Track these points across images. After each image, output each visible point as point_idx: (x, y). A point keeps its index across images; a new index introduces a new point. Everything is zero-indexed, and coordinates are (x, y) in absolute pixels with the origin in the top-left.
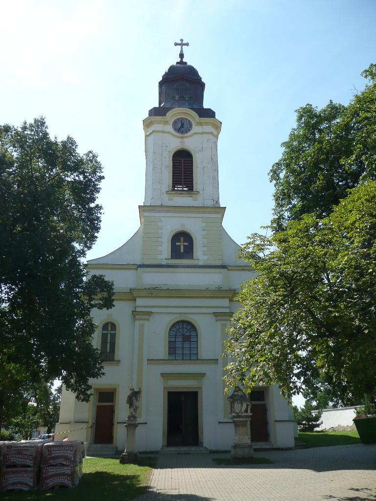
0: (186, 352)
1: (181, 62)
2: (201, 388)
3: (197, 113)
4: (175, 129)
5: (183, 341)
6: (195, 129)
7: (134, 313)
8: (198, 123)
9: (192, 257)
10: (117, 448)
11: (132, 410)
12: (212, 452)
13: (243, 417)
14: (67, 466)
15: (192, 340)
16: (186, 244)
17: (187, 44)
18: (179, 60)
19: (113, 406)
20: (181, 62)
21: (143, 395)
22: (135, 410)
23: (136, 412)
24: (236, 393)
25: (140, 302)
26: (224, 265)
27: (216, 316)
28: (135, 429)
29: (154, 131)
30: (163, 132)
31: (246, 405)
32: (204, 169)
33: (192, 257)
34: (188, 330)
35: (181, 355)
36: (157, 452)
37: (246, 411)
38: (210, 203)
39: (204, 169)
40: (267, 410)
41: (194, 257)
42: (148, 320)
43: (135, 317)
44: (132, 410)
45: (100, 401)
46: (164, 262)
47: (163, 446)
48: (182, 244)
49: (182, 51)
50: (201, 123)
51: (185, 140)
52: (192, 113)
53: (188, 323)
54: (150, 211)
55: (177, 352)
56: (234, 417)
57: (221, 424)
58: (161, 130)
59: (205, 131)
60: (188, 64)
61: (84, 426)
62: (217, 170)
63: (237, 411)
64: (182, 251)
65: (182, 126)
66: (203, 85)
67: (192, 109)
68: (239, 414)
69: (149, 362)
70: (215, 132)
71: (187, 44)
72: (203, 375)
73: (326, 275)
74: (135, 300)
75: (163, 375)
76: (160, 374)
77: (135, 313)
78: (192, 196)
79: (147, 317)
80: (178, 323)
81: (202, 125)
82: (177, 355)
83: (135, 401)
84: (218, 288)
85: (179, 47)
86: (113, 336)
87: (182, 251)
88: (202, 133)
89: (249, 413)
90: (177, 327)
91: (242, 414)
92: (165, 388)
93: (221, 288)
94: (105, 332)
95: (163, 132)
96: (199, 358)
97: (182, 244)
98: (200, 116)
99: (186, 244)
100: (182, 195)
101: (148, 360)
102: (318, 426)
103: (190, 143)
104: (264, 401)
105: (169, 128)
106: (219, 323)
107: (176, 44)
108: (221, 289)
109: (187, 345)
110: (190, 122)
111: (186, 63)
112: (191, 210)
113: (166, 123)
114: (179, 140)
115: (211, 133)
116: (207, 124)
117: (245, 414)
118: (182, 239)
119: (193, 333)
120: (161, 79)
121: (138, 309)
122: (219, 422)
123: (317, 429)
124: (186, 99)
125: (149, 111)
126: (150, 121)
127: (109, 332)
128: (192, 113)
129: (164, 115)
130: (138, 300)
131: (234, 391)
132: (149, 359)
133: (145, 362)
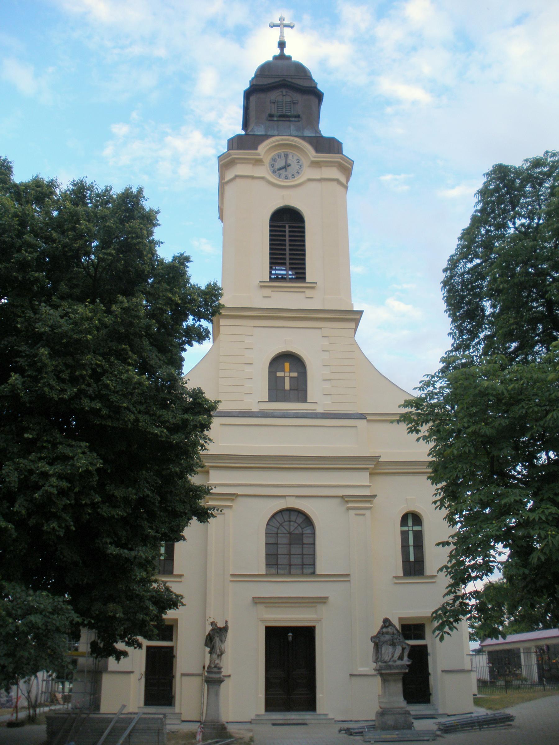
0: (296, 560)
1: (282, 57)
5: (290, 544)
9: (303, 398)
13: (397, 667)
14: (133, 413)
15: (305, 541)
16: (295, 374)
18: (277, 52)
20: (282, 57)
23: (221, 660)
24: (384, 630)
28: (220, 685)
31: (400, 648)
33: (303, 398)
34: (299, 525)
35: (299, 556)
37: (401, 658)
41: (309, 400)
46: (255, 408)
49: (282, 35)
53: (299, 512)
55: (280, 562)
57: (354, 679)
60: (293, 59)
63: (387, 658)
64: (287, 387)
66: (319, 96)
67: (303, 138)
70: (343, 179)
72: (323, 600)
75: (257, 601)
76: (251, 598)
80: (281, 512)
81: (320, 167)
82: (304, 546)
83: (217, 639)
86: (418, 536)
87: (287, 387)
90: (286, 517)
91: (394, 664)
94: (405, 529)
98: (317, 150)
99: (295, 374)
105: (263, 171)
106: (352, 513)
109: (296, 550)
111: (289, 58)
113: (258, 162)
115: (337, 181)
117: (399, 663)
118: (287, 365)
119: (308, 531)
120: (248, 86)
127: (410, 528)
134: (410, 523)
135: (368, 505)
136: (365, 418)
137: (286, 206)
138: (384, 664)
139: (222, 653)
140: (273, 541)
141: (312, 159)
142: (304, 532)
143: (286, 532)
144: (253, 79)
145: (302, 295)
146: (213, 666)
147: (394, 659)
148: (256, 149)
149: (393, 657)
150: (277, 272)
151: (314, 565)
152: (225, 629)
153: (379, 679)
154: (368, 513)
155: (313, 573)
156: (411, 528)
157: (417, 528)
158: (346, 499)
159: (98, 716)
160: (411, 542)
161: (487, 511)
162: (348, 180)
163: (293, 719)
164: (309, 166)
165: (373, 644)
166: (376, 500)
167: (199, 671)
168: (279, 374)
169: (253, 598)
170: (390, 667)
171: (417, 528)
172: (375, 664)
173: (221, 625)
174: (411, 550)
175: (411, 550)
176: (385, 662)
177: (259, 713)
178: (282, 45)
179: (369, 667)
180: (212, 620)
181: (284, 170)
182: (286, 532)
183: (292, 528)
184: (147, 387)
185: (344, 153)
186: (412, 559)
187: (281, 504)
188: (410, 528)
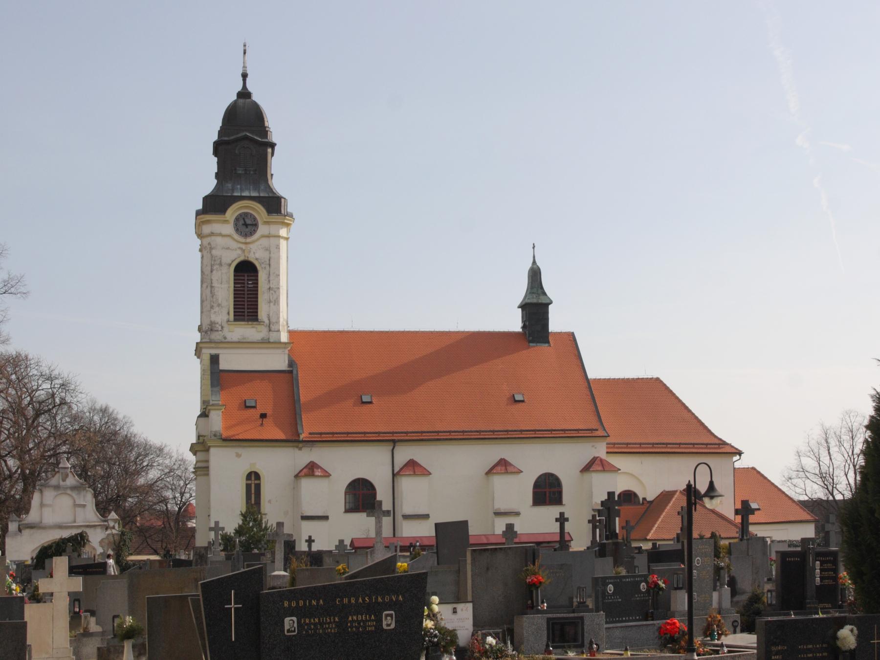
3: (264, 206)
4: (237, 230)
6: (262, 229)
8: (265, 222)
52: (258, 207)
65: (246, 225)
81: (269, 225)
86: (258, 487)
94: (249, 482)
103: (255, 252)
105: (229, 229)
112: (240, 345)
113: (226, 222)
120: (219, 129)
122: (326, 518)
125: (203, 198)
127: (253, 482)
134: (253, 478)
141: (265, 220)
144: (221, 127)
148: (225, 214)
156: (253, 482)
157: (257, 482)
159: (194, 561)
161: (423, 633)
164: (262, 224)
167: (261, 419)
171: (257, 482)
174: (253, 496)
175: (253, 496)
181: (243, 223)
184: (124, 527)
188: (253, 482)
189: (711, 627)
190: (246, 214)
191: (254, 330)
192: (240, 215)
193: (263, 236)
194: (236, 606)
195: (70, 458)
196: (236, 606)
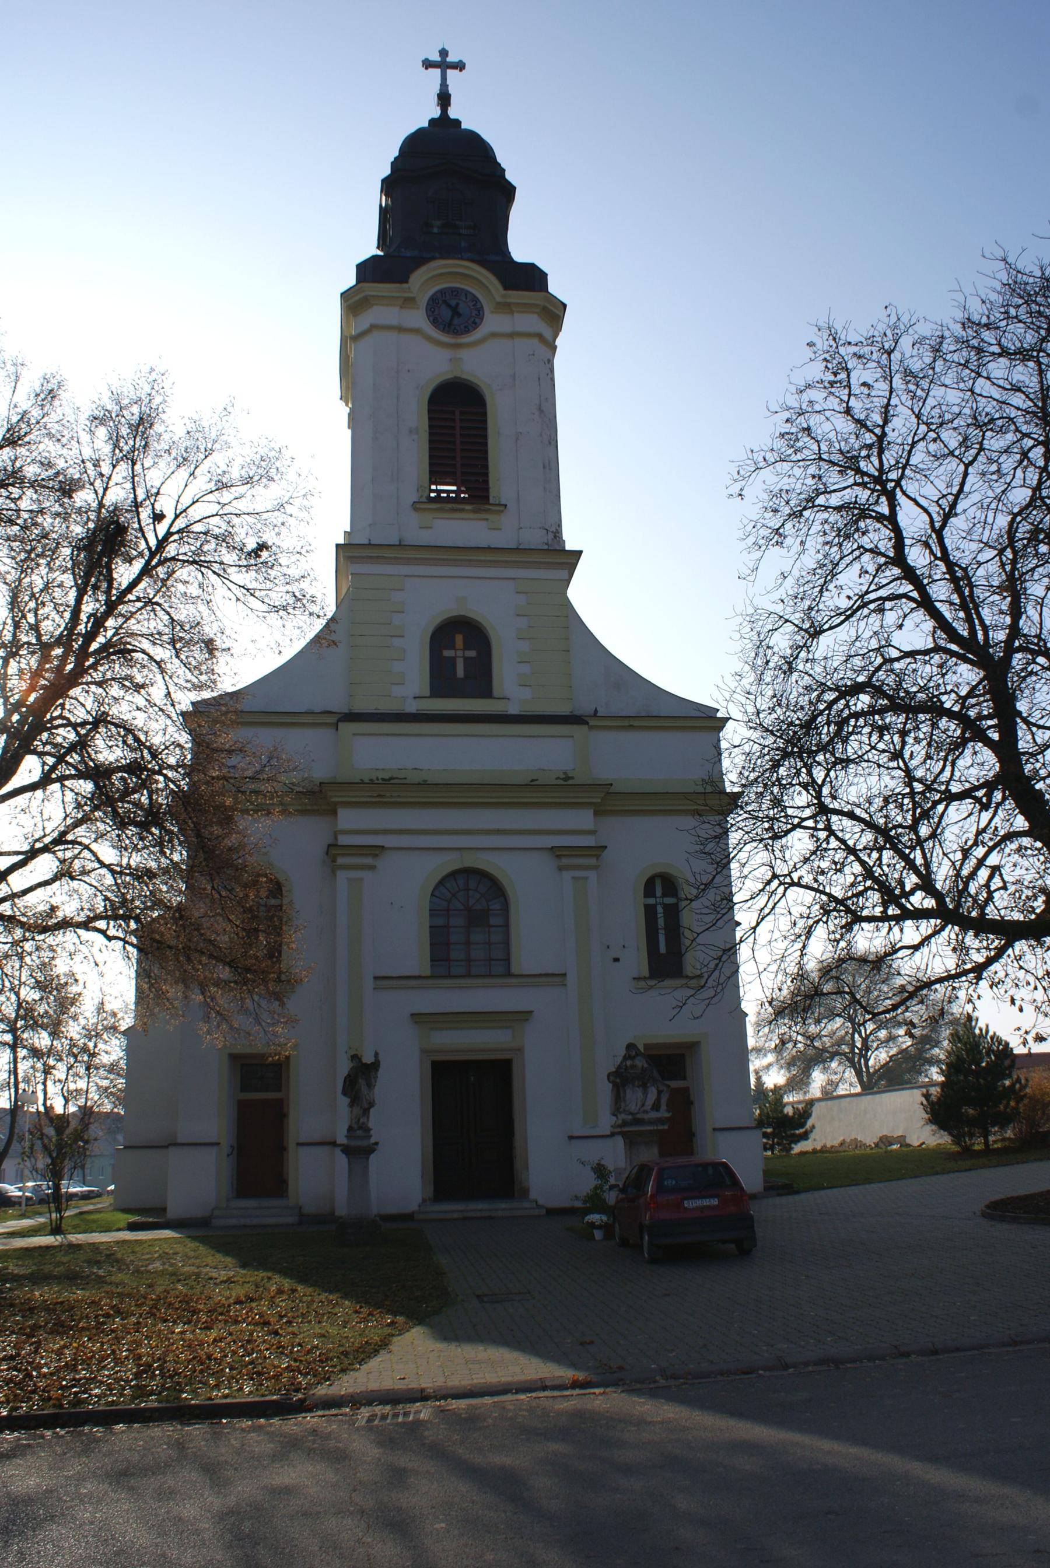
2: (520, 1050)
4: (435, 322)
6: (492, 322)
7: (333, 851)
8: (498, 304)
9: (485, 690)
10: (300, 1208)
11: (357, 1110)
12: (552, 1212)
13: (651, 1122)
15: (493, 921)
16: (472, 654)
17: (460, 66)
18: (436, 113)
19: (686, 1090)
21: (382, 1073)
22: (366, 1112)
24: (629, 1063)
25: (348, 819)
26: (577, 713)
27: (558, 856)
28: (368, 1158)
29: (373, 327)
30: (400, 329)
31: (655, 1092)
32: (517, 439)
36: (408, 1217)
37: (656, 1107)
38: (534, 538)
39: (517, 439)
40: (692, 1103)
42: (372, 868)
43: (334, 861)
44: (357, 1110)
45: (244, 1088)
46: (412, 707)
47: (424, 1201)
48: (459, 654)
50: (508, 305)
51: (464, 354)
54: (370, 559)
56: (625, 1123)
57: (574, 1141)
58: (394, 322)
59: (518, 329)
60: (463, 126)
61: (214, 1150)
62: (553, 443)
63: (633, 1107)
64: (460, 673)
66: (508, 192)
68: (639, 1116)
69: (380, 983)
71: (460, 66)
72: (525, 1016)
73: (88, 607)
74: (334, 813)
75: (418, 1018)
77: (333, 851)
78: (487, 519)
79: (368, 861)
80: (454, 874)
83: (362, 1082)
84: (563, 779)
85: (437, 72)
87: (460, 673)
88: (512, 335)
89: (663, 1113)
91: (646, 1117)
92: (424, 1052)
93: (572, 778)
94: (651, 901)
95: (400, 329)
96: (515, 969)
97: (459, 654)
99: (472, 654)
100: (453, 510)
101: (376, 978)
102: (805, 1136)
104: (684, 1078)
105: (418, 318)
106: (567, 875)
107: (428, 64)
108: (570, 782)
110: (476, 300)
111: (458, 122)
113: (409, 302)
114: (445, 354)
115: (540, 336)
116: (526, 308)
118: (459, 639)
119: (495, 906)
120: (387, 171)
121: (343, 840)
122: (571, 1138)
123: (797, 1148)
124: (463, 231)
126: (362, 295)
128: (474, 270)
129: (404, 279)
130: (341, 812)
131: (625, 1058)
132: (378, 975)
133: (369, 983)
135: (592, 861)
136: (587, 723)
137: (456, 378)
138: (630, 1117)
139: (372, 1104)
140: (440, 922)
142: (492, 907)
143: (462, 907)
144: (396, 159)
145: (484, 524)
146: (355, 1126)
147: (645, 1108)
149: (643, 1105)
150: (439, 487)
151: (507, 960)
152: (375, 1066)
153: (620, 1141)
154: (592, 875)
155: (509, 974)
158: (558, 853)
160: (661, 922)
162: (556, 336)
163: (480, 1210)
164: (492, 312)
165: (611, 1085)
166: (606, 854)
168: (448, 653)
169: (412, 1015)
170: (638, 1122)
172: (615, 1118)
173: (368, 1059)
174: (662, 938)
175: (662, 938)
176: (631, 1114)
177: (457, 71)
178: (444, 99)
179: (606, 1122)
180: (353, 1052)
182: (462, 907)
183: (471, 902)
185: (550, 290)
186: (663, 949)
187: (453, 863)
189: (953, 972)
190: (455, 292)
191: (483, 524)
192: (442, 292)
193: (494, 335)
194: (660, 909)
195: (837, 688)
196: (660, 909)
